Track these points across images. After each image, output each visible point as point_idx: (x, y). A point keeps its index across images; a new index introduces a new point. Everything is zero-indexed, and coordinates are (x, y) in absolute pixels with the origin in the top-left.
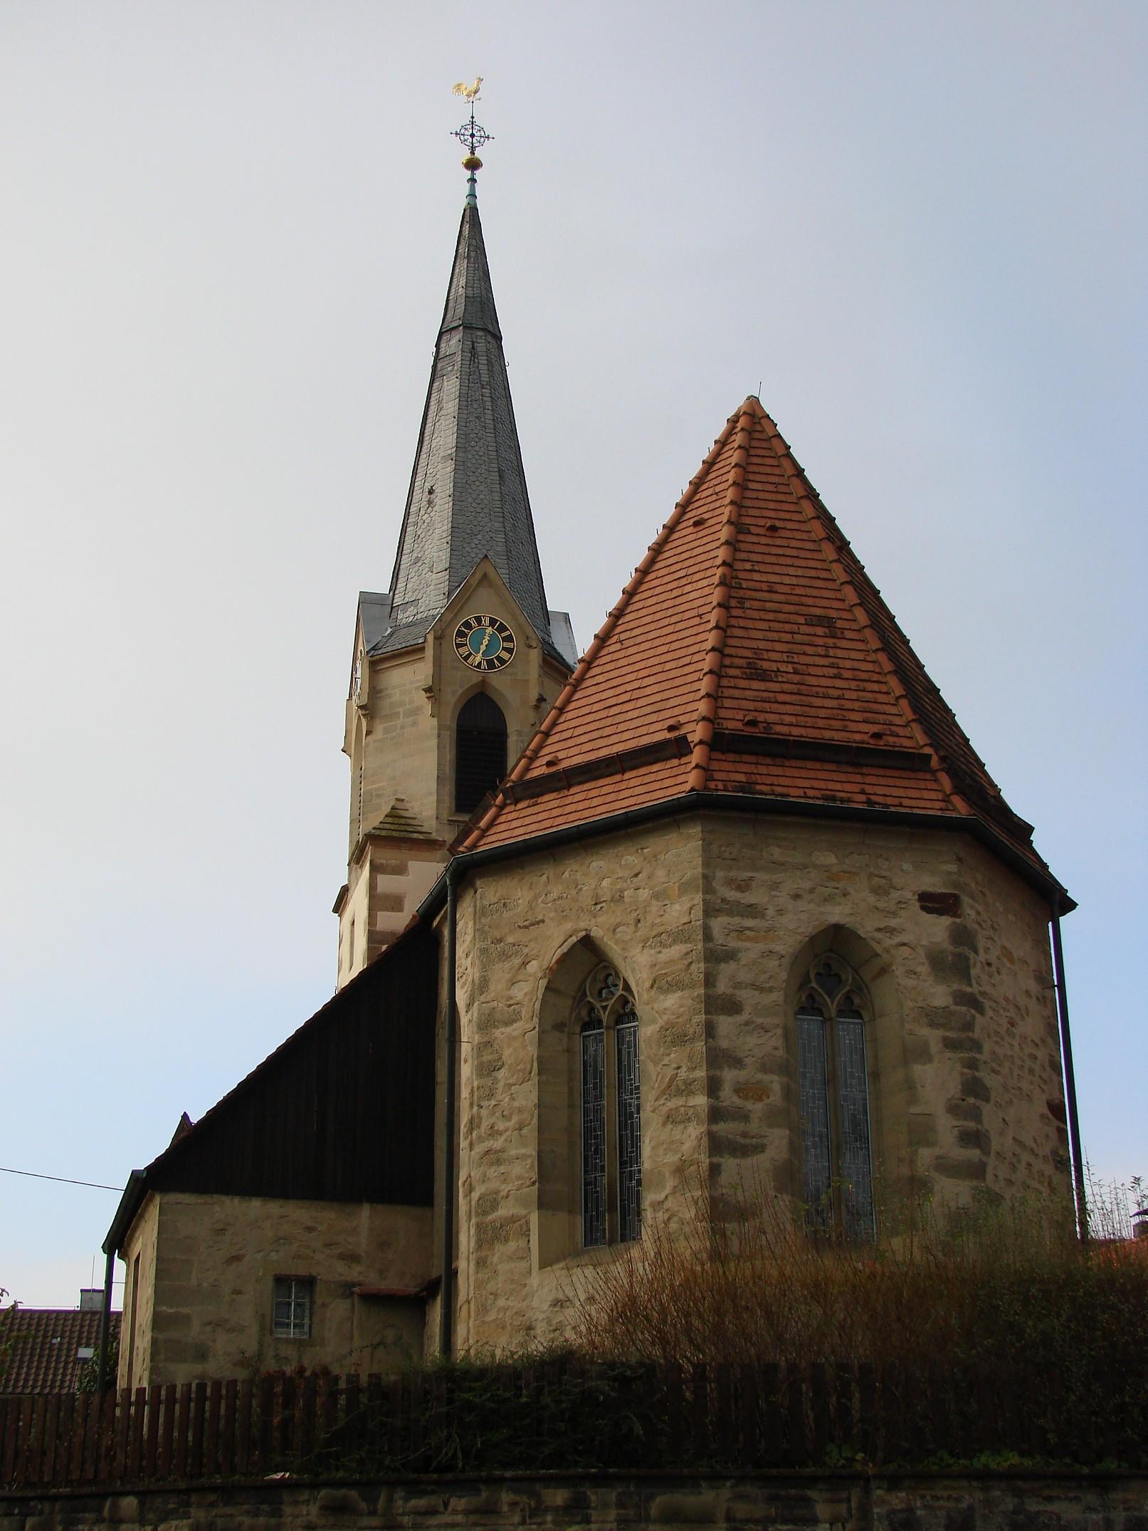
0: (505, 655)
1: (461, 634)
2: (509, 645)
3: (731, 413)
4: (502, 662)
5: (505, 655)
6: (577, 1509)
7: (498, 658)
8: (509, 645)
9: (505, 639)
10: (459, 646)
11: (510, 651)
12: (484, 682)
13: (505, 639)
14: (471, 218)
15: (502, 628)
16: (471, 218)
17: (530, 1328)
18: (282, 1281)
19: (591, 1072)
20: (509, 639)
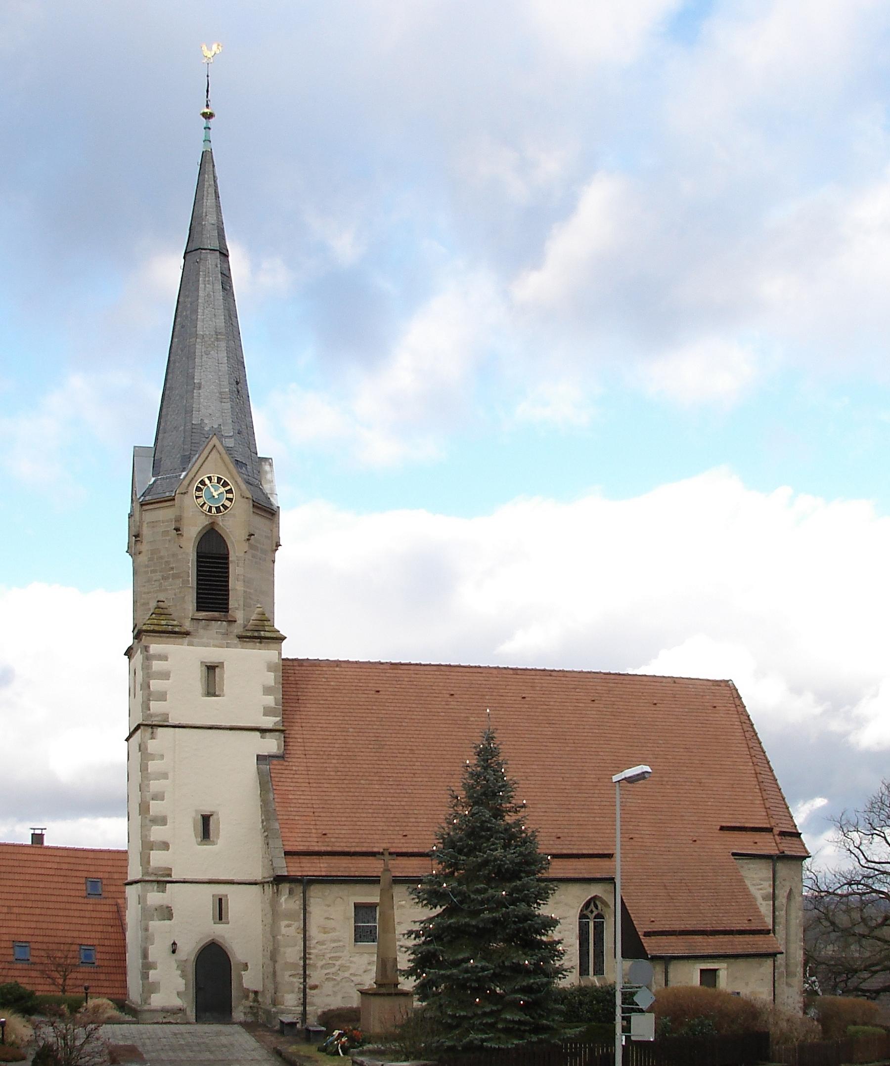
0: (228, 503)
1: (198, 489)
2: (230, 496)
3: (289, 524)
4: (226, 508)
5: (228, 503)
6: (267, 691)
7: (223, 505)
8: (230, 496)
9: (227, 492)
10: (197, 497)
11: (230, 500)
12: (213, 523)
13: (227, 492)
14: (206, 160)
15: (225, 484)
16: (206, 160)
17: (175, 1034)
18: (169, 909)
19: (229, 310)
20: (230, 491)
